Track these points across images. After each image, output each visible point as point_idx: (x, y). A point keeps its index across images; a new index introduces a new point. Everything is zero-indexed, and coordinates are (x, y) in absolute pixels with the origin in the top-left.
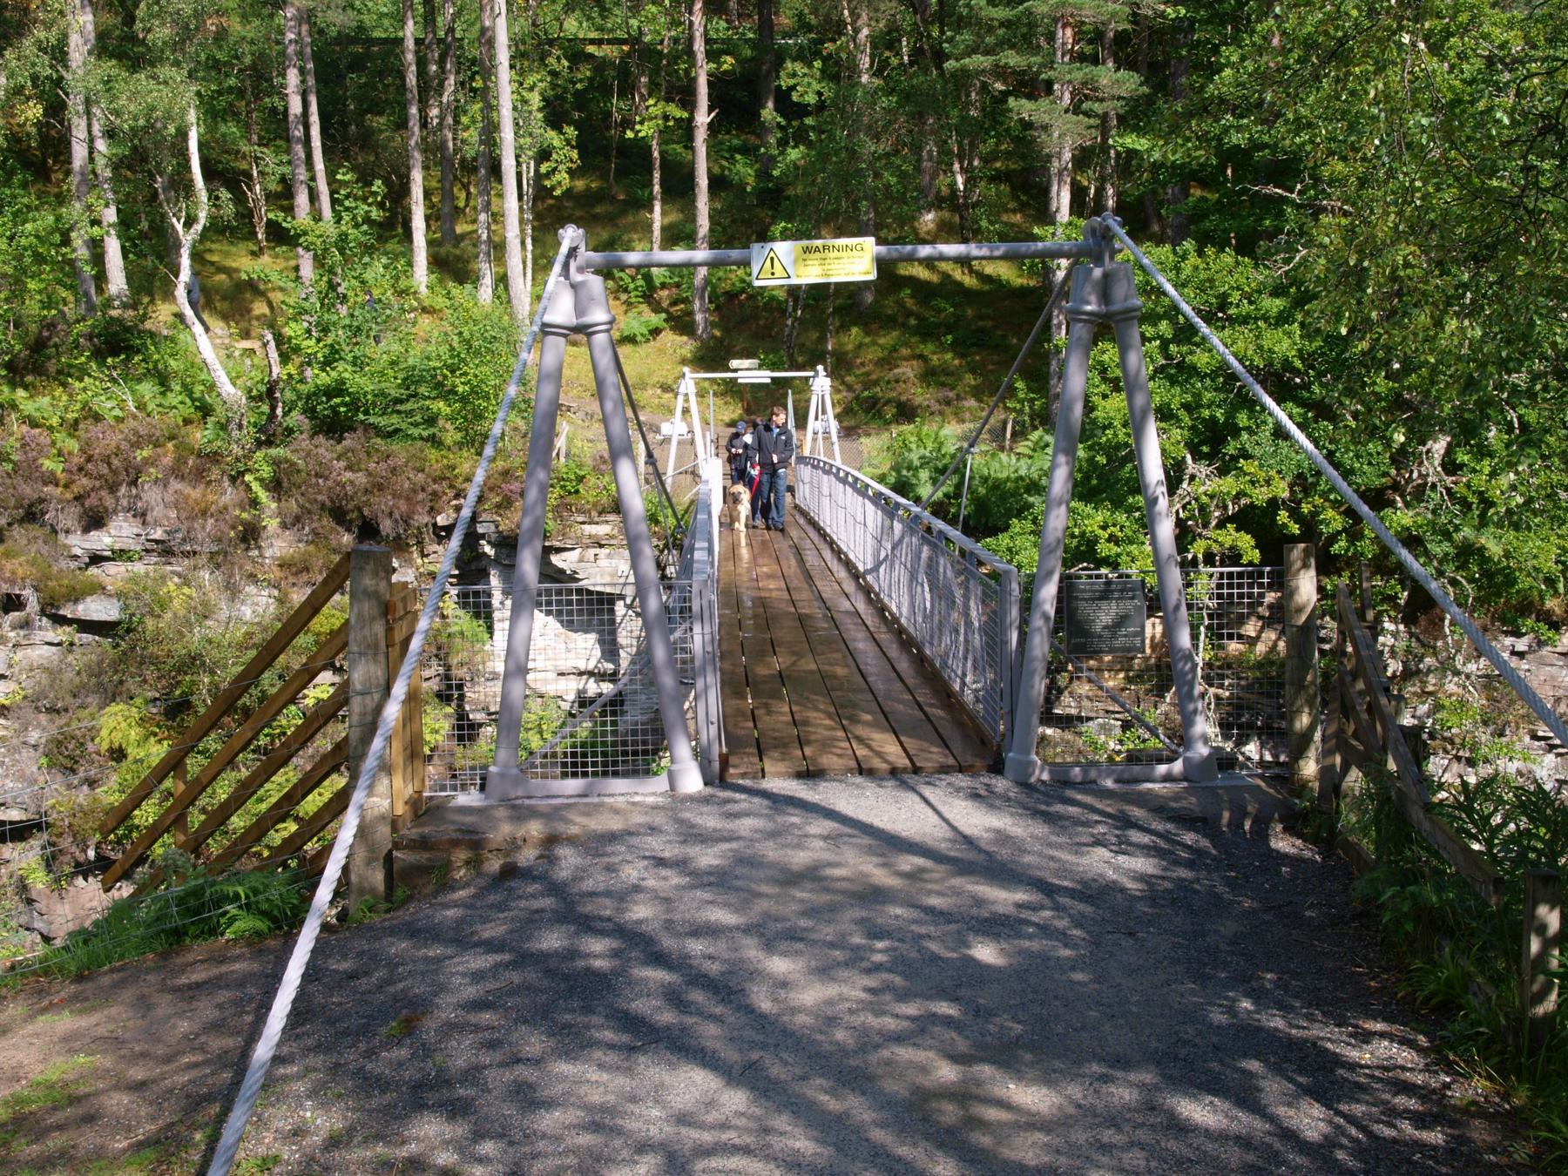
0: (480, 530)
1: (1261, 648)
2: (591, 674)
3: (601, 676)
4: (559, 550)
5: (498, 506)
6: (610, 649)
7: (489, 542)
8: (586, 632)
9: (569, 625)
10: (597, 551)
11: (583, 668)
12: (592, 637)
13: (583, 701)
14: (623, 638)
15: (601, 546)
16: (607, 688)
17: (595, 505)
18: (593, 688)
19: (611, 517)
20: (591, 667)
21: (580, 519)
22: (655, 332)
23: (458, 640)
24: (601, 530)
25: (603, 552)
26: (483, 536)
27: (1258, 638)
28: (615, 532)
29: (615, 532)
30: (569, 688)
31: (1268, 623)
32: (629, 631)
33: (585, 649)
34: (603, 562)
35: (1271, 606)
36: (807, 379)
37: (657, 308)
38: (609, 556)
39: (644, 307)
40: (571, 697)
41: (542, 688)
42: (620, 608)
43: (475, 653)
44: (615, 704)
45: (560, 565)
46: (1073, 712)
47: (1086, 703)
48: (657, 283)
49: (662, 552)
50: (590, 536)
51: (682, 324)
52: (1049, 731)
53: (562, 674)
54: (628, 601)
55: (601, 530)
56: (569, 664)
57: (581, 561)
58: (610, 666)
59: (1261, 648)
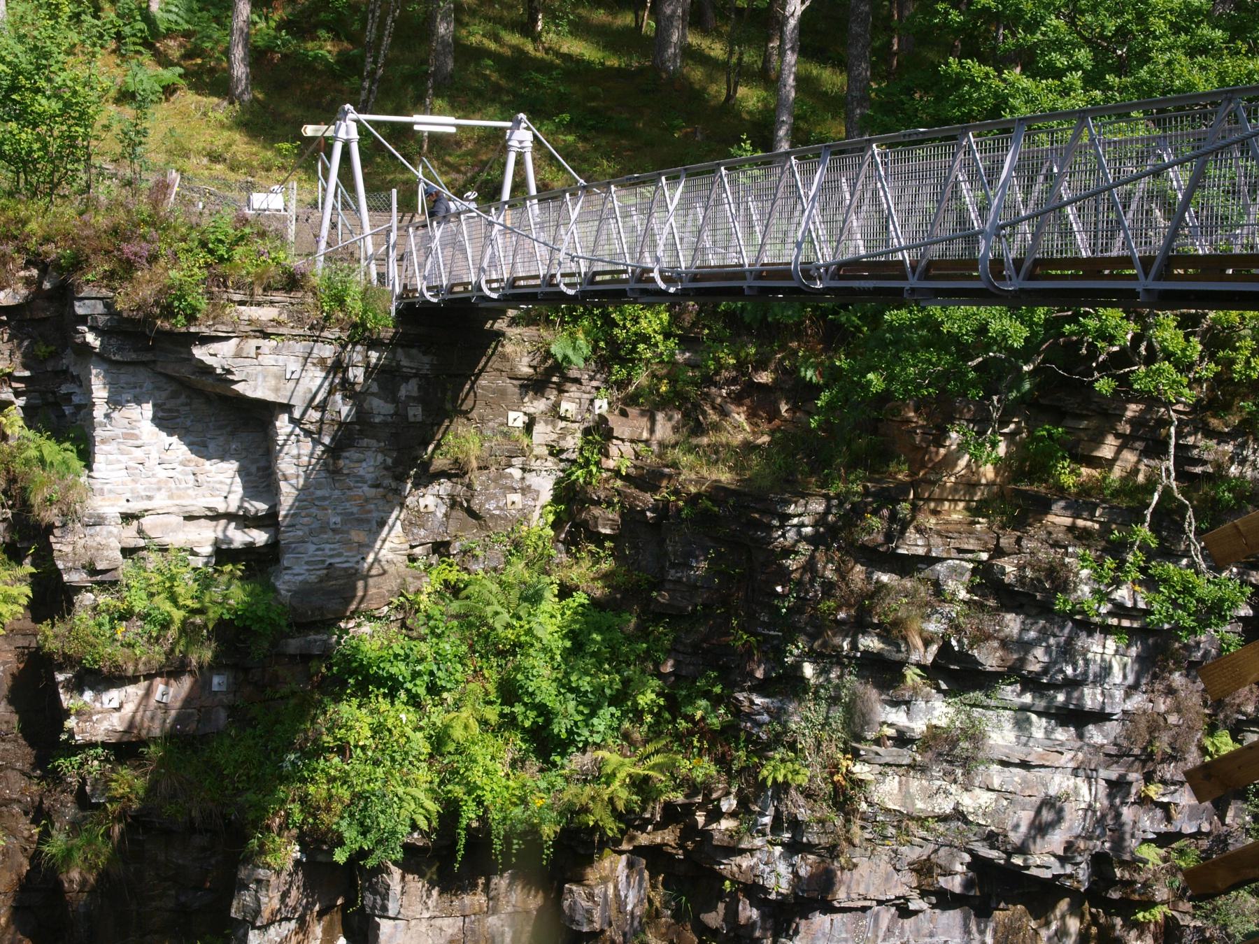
0: (80, 309)
1: (1117, 473)
2: (229, 517)
3: (244, 520)
4: (205, 340)
5: (111, 275)
6: (261, 478)
7: (92, 329)
8: (223, 459)
9: (200, 448)
10: (260, 342)
11: (222, 508)
12: (232, 466)
13: (223, 554)
14: (286, 465)
15: (266, 336)
16: (260, 537)
17: (259, 277)
18: (239, 537)
19: (279, 297)
20: (233, 508)
21: (237, 297)
22: (169, 90)
23: (37, 470)
24: (265, 314)
25: (267, 345)
26: (83, 319)
27: (1115, 460)
28: (284, 317)
29: (284, 317)
30: (204, 537)
31: (1126, 442)
32: (295, 457)
33: (222, 482)
34: (268, 359)
35: (1131, 421)
36: (503, 130)
37: (163, 60)
38: (276, 351)
39: (147, 58)
40: (207, 549)
41: (169, 539)
42: (283, 424)
43: (68, 488)
44: (255, 563)
45: (209, 361)
46: (921, 551)
47: (935, 540)
48: (162, 28)
49: (344, 347)
50: (251, 322)
51: (211, 81)
52: (885, 578)
53: (189, 518)
54: (297, 415)
55: (265, 314)
56: (199, 503)
57: (238, 355)
58: (261, 507)
59: (1117, 473)
